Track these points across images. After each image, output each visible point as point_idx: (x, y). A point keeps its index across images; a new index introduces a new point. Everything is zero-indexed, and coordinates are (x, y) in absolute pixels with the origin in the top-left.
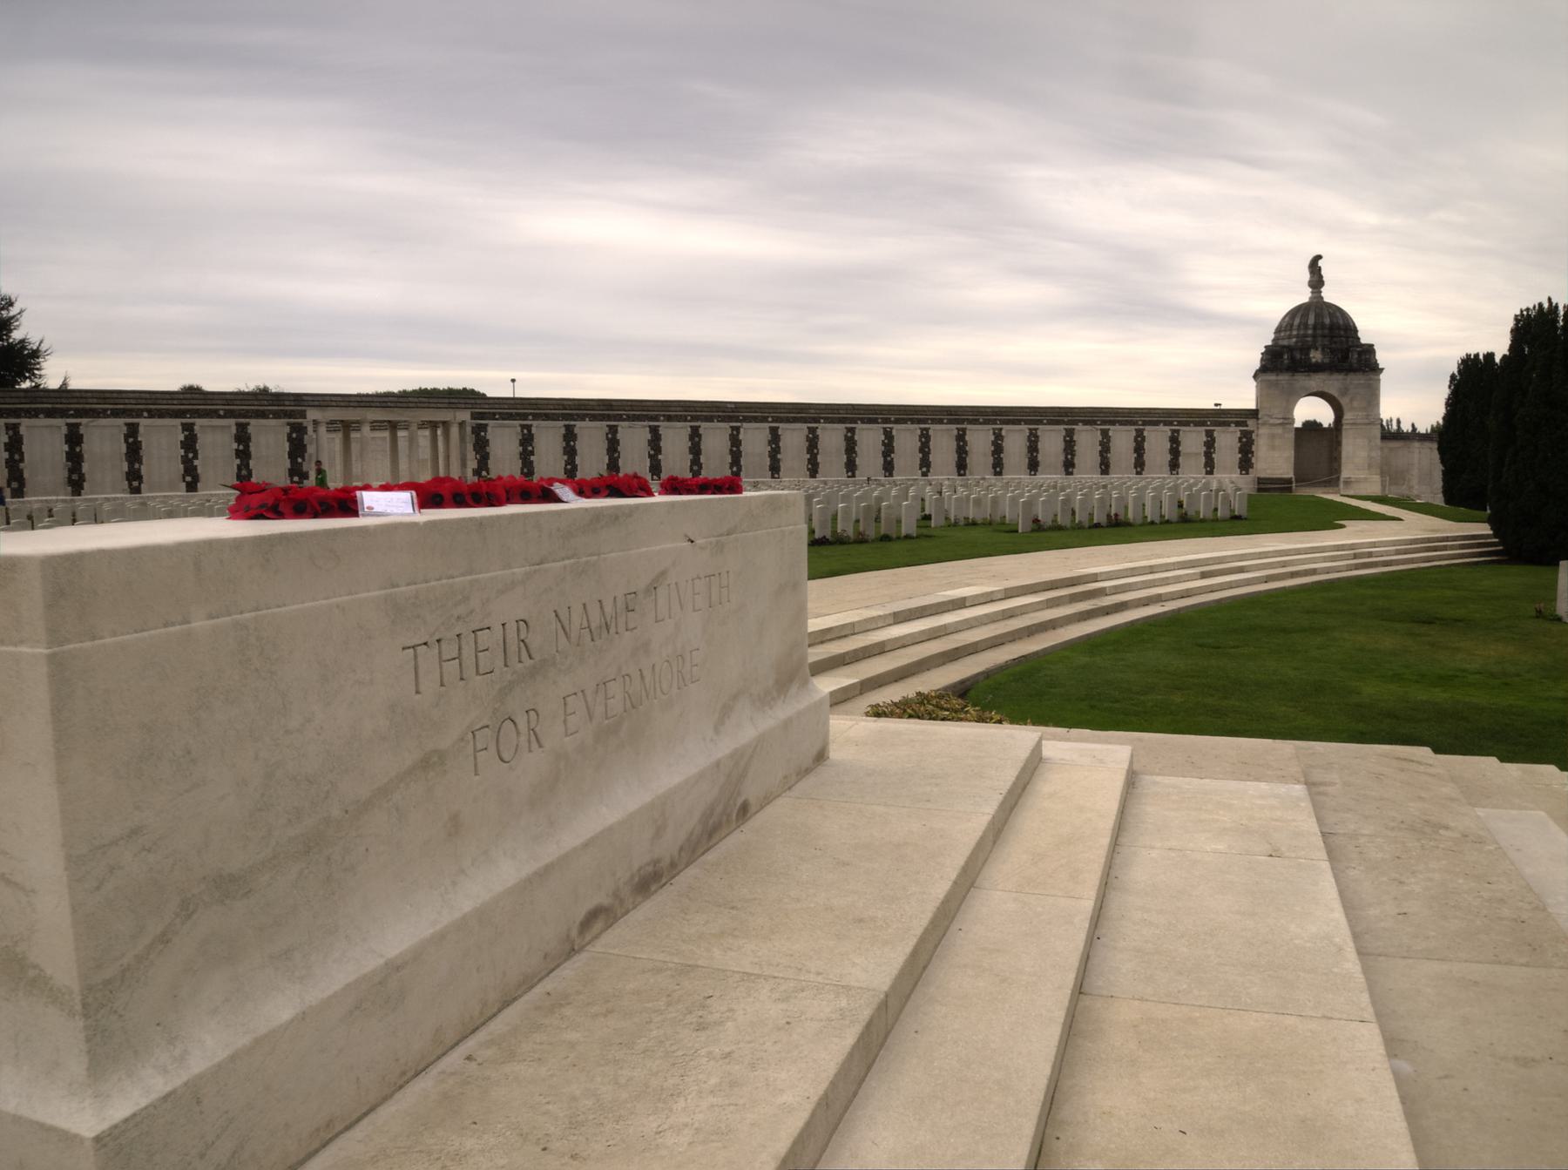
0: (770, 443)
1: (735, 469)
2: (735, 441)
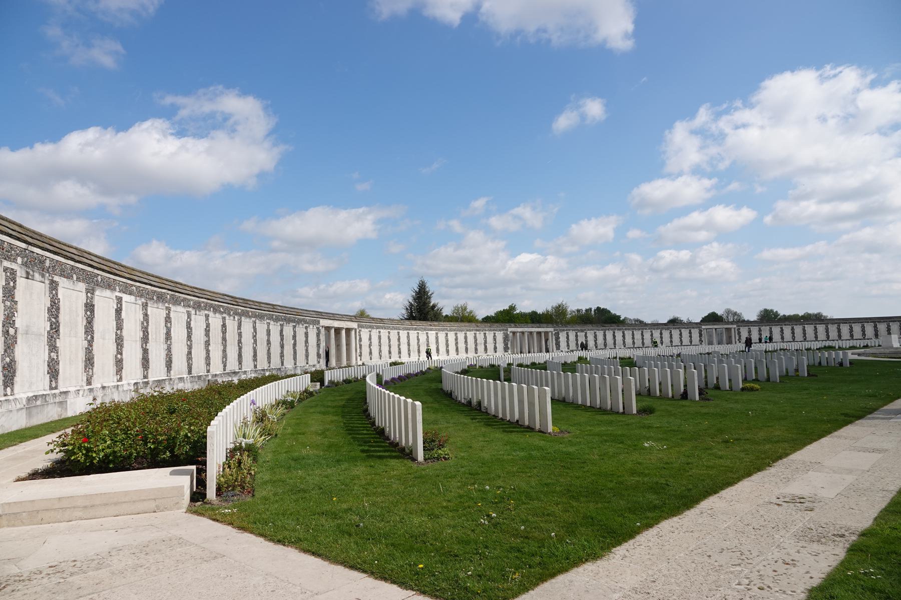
2: (804, 330)
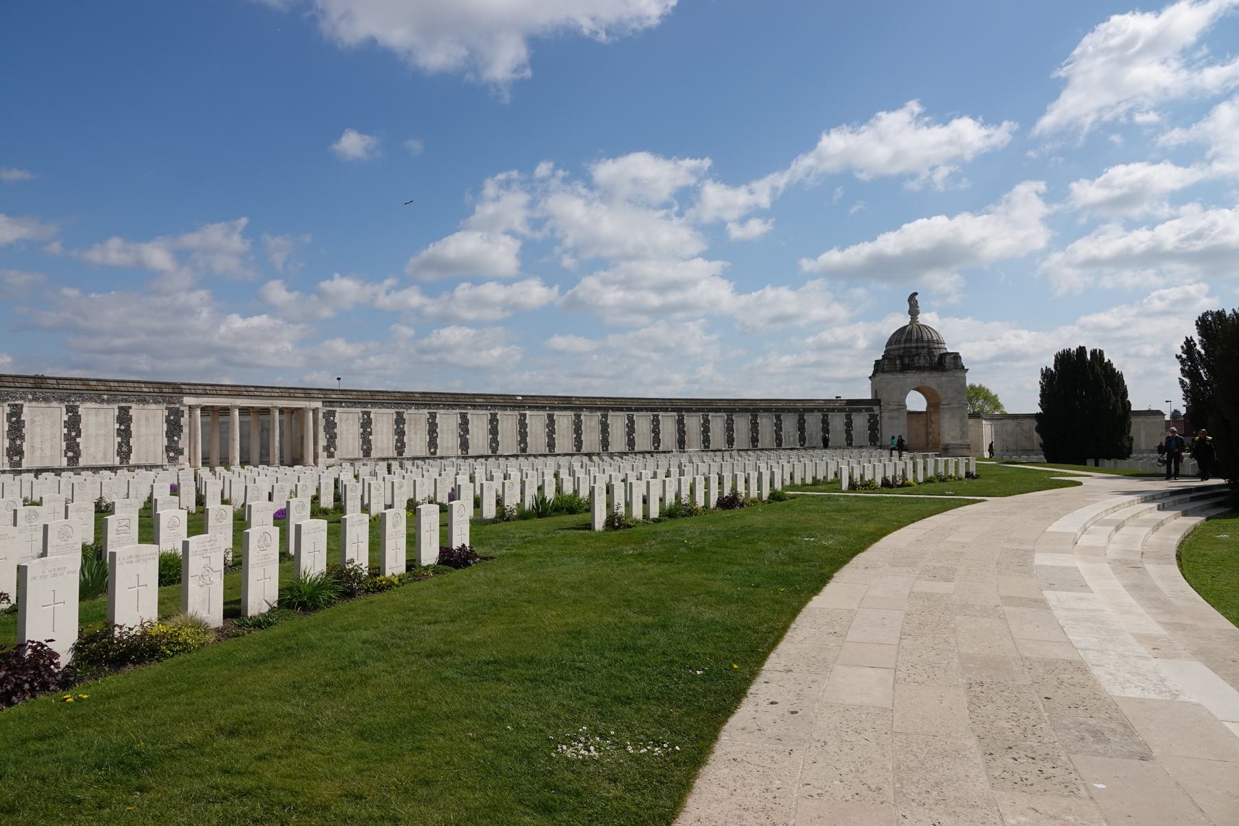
0: (548, 426)
1: (522, 445)
2: (523, 424)
